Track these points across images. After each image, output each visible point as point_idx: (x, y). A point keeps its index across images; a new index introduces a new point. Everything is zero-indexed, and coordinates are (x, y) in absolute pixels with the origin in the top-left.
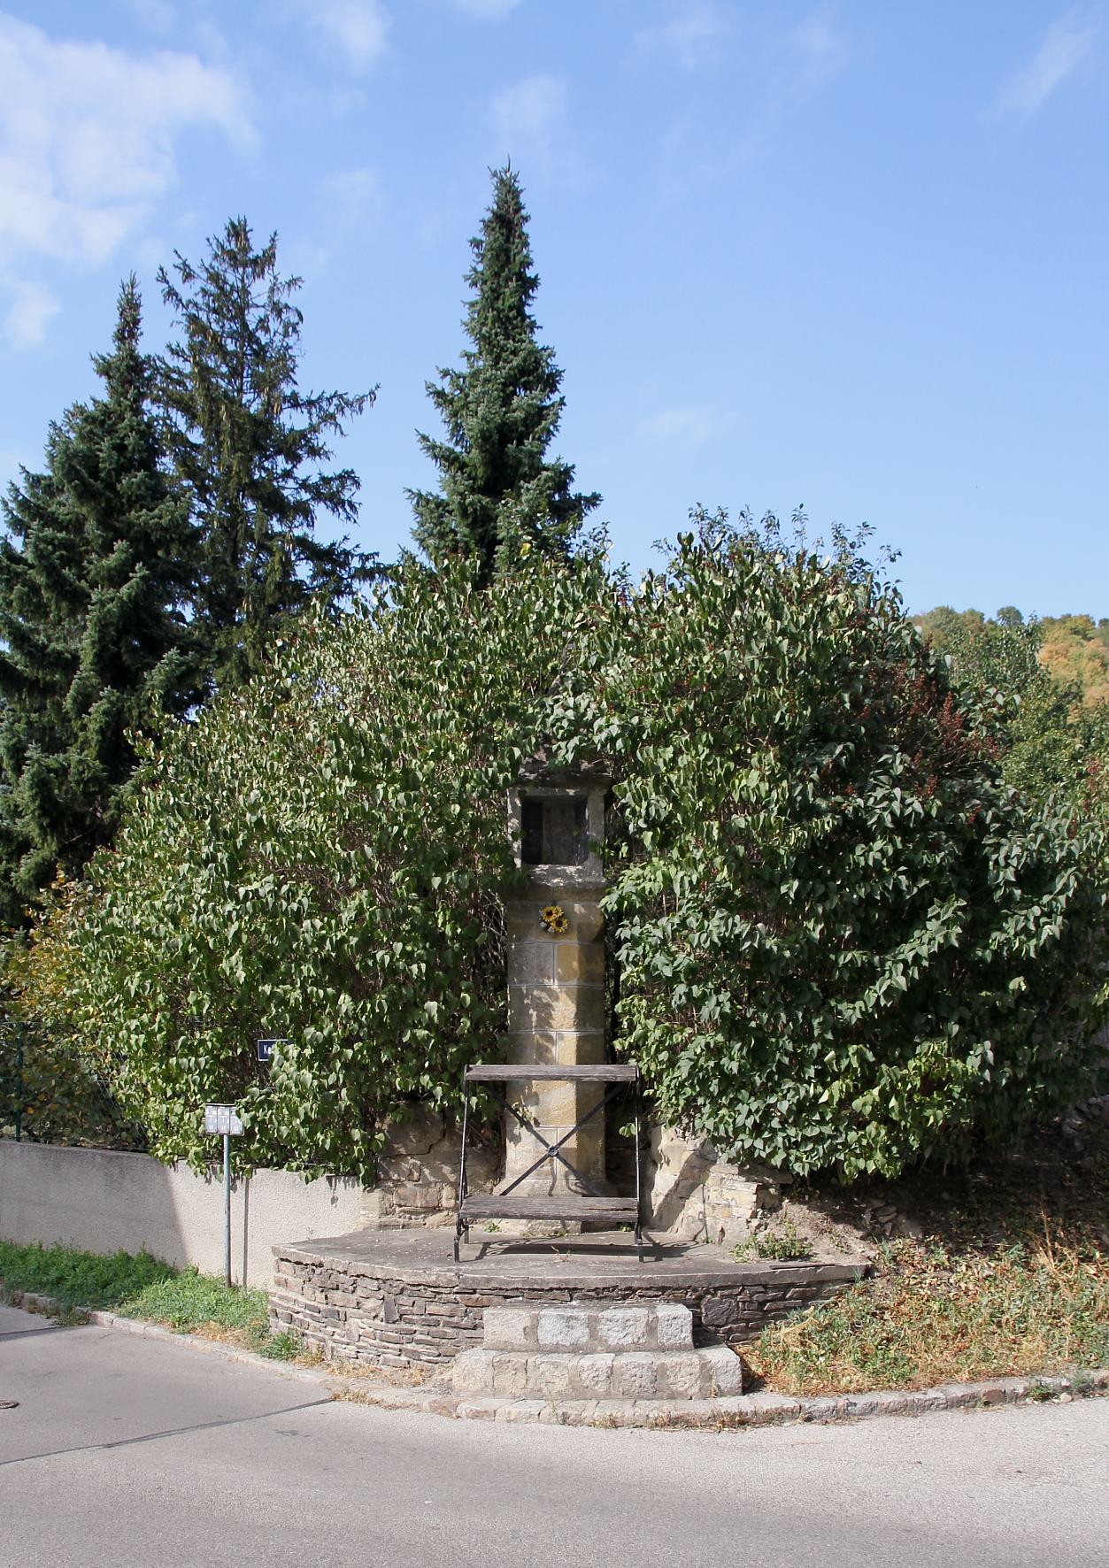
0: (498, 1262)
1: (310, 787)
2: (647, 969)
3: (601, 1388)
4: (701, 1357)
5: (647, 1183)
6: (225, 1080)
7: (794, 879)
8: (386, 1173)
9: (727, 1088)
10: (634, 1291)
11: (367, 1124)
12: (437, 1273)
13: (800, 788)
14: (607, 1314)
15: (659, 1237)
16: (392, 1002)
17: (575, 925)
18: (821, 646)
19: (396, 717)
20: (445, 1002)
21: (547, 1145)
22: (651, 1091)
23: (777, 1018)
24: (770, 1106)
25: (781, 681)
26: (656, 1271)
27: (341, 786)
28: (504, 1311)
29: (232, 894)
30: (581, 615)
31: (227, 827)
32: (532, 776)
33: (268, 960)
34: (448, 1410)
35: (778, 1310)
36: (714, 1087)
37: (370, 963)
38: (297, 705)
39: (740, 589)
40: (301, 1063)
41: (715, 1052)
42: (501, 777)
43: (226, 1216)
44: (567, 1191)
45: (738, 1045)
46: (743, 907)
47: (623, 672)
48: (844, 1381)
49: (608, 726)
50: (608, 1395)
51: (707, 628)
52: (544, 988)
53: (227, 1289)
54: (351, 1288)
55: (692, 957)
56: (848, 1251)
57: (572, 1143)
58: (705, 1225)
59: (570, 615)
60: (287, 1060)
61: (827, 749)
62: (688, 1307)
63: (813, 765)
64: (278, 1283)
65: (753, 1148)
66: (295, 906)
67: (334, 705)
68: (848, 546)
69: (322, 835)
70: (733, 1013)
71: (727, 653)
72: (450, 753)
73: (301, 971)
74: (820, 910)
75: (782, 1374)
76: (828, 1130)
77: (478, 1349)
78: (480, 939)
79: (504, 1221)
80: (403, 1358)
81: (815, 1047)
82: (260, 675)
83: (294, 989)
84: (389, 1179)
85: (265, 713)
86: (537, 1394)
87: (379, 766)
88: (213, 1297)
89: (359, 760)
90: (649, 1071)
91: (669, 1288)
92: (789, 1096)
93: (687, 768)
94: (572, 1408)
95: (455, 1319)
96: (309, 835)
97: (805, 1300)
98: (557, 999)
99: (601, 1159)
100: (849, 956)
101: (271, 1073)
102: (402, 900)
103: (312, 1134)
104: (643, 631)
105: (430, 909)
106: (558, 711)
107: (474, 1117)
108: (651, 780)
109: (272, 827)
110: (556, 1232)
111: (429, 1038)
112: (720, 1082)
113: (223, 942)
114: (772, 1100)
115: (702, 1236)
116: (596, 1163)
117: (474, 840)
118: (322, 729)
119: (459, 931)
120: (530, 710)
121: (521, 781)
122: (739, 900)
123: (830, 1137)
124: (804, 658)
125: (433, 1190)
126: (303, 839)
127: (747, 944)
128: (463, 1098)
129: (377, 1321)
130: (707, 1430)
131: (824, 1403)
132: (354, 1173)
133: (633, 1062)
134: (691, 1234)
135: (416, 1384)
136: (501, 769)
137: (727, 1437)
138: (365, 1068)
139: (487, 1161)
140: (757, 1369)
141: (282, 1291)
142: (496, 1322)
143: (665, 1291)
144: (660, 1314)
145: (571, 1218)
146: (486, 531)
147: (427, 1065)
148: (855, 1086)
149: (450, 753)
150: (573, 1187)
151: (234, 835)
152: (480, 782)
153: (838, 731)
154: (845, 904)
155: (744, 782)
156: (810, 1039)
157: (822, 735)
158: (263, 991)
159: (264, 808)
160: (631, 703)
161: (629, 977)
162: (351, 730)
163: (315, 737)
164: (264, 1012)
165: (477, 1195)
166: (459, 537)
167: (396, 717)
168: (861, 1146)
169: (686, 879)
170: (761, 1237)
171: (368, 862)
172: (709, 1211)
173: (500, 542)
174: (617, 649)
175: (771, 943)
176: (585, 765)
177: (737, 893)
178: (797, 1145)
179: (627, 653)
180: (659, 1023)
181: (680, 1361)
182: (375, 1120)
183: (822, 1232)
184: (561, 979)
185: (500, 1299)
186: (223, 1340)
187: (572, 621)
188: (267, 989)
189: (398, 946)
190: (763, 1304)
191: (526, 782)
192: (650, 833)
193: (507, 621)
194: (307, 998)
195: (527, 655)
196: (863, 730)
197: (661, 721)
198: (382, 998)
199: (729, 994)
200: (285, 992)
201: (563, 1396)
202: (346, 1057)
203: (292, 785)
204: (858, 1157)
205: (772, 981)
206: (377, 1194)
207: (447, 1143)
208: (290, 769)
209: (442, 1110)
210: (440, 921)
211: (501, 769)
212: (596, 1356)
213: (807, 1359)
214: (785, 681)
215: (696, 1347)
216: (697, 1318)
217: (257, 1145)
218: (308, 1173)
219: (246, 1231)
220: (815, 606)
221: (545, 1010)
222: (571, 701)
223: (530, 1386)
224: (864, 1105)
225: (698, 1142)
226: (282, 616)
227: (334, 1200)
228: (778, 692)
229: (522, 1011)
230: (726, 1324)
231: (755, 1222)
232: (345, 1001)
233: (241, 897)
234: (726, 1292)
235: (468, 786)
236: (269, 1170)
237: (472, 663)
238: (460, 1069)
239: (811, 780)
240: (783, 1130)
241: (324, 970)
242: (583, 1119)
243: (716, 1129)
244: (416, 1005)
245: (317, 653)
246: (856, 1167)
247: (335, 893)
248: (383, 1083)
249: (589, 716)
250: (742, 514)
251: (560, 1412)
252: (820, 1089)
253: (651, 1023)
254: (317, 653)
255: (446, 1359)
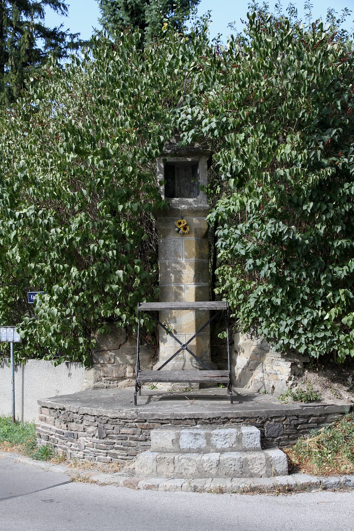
0: (157, 405)
1: (52, 158)
2: (232, 251)
3: (213, 472)
4: (266, 454)
5: (233, 363)
6: (11, 313)
7: (310, 201)
8: (97, 360)
9: (274, 313)
10: (228, 419)
11: (87, 334)
12: (127, 412)
13: (313, 153)
14: (215, 432)
15: (240, 390)
16: (99, 271)
17: (193, 230)
18: (324, 74)
19: (97, 120)
20: (126, 270)
21: (181, 343)
22: (234, 315)
23: (301, 275)
24: (297, 322)
25: (303, 94)
26: (239, 409)
27: (69, 157)
28: (161, 431)
29: (12, 216)
30: (193, 63)
31: (8, 180)
32: (169, 151)
33: (32, 250)
34: (133, 485)
35: (305, 429)
36: (268, 312)
37: (87, 251)
38: (43, 114)
39: (281, 43)
40: (51, 303)
41: (267, 294)
42: (154, 152)
43: (12, 385)
44: (191, 367)
45: (281, 290)
46: (283, 217)
47: (218, 93)
48: (343, 468)
49: (210, 123)
50: (217, 476)
51: (263, 65)
52: (178, 263)
53: (13, 424)
54: (80, 421)
55: (255, 245)
56: (341, 398)
57: (194, 342)
58: (264, 384)
59: (187, 64)
60: (44, 302)
61: (327, 132)
62: (257, 427)
63: (320, 141)
64: (41, 420)
65: (289, 344)
66: (46, 221)
67: (63, 114)
68: (336, 23)
69: (59, 184)
70: (277, 273)
71: (274, 80)
72: (127, 139)
73: (50, 256)
74: (324, 218)
75: (309, 464)
76: (329, 334)
77: (148, 452)
78: (144, 237)
79: (159, 383)
80: (108, 457)
81: (321, 290)
82: (22, 97)
83: (47, 265)
84: (99, 363)
85: (26, 118)
86: (180, 476)
87: (89, 146)
88: (6, 428)
89: (78, 143)
90: (233, 304)
91: (247, 418)
92: (308, 316)
93: (254, 143)
94: (199, 482)
95: (136, 436)
96: (52, 184)
97: (319, 423)
98: (185, 268)
99: (209, 351)
100: (340, 243)
101: (35, 309)
102: (102, 218)
103: (57, 341)
104: (228, 70)
105: (117, 223)
106: (183, 116)
107: (143, 329)
108: (233, 151)
109: (32, 180)
110: (186, 389)
111: (119, 289)
112: (271, 309)
113: (8, 242)
114: (299, 318)
115: (263, 390)
116: (206, 352)
117: (139, 185)
118: (57, 127)
119: (133, 233)
120: (168, 116)
121: (163, 154)
122: (281, 214)
123: (330, 337)
124: (315, 81)
125: (121, 368)
126: (49, 186)
127: (286, 237)
128: (137, 320)
129: (94, 438)
130: (271, 494)
131: (333, 480)
132: (80, 360)
133: (224, 300)
134: (257, 389)
135: (116, 471)
136: (154, 147)
137: (282, 498)
138: (85, 305)
139: (149, 352)
140: (295, 461)
141: (43, 424)
142: (157, 437)
143: (246, 420)
144: (243, 432)
145: (195, 381)
146: (139, 19)
147: (118, 303)
148: (343, 311)
149: (127, 139)
150: (195, 365)
151: (12, 184)
152: (143, 154)
153: (334, 122)
154: (337, 214)
155: (283, 151)
156: (319, 287)
157: (324, 126)
158: (31, 267)
159: (27, 170)
160: (222, 110)
161: (222, 255)
162: (73, 127)
163: (54, 131)
164: (30, 278)
165: (145, 370)
166: (124, 22)
167: (97, 120)
168: (346, 342)
169: (253, 204)
170: (294, 390)
171: (83, 197)
172: (266, 377)
173: (147, 25)
174: (214, 80)
175: (298, 236)
176: (197, 145)
177: (279, 210)
178: (312, 342)
179: (220, 83)
180: (238, 279)
181: (255, 456)
182: (90, 333)
183: (326, 387)
184: (186, 257)
185: (159, 425)
186: (12, 451)
187: (189, 67)
188: (32, 265)
189: (101, 242)
190: (296, 426)
191: (166, 155)
192: (233, 180)
193: (153, 67)
194: (54, 270)
195: (164, 86)
196: (348, 121)
197: (238, 120)
198: (93, 268)
199: (275, 263)
200: (42, 267)
201: (194, 476)
202: (75, 300)
203: (42, 157)
204: (345, 348)
205: (299, 256)
206: (92, 371)
207: (128, 343)
208: (41, 149)
209: (126, 327)
210: (123, 228)
211: (154, 147)
212: (210, 454)
213: (322, 455)
214: (305, 94)
215: (263, 449)
216: (262, 433)
217: (28, 347)
218: (56, 361)
219: (23, 392)
220: (321, 52)
221: (178, 274)
222: (189, 110)
223: (176, 471)
224: (348, 320)
225: (259, 341)
226: (30, 68)
227: (70, 375)
228: (302, 100)
229: (167, 274)
230: (278, 436)
231: (291, 383)
232: (74, 271)
233: (17, 216)
234: (277, 420)
235: (136, 157)
236: (35, 360)
237: (136, 90)
238: (135, 305)
239: (320, 149)
240: (305, 334)
241: (63, 255)
242: (199, 330)
243: (269, 334)
244: (111, 272)
245: (53, 86)
246: (345, 353)
247: (67, 214)
248: (95, 313)
249: (200, 118)
250: (276, 6)
251: (192, 485)
252: (324, 312)
253: (234, 279)
254: (53, 86)
255: (131, 457)
